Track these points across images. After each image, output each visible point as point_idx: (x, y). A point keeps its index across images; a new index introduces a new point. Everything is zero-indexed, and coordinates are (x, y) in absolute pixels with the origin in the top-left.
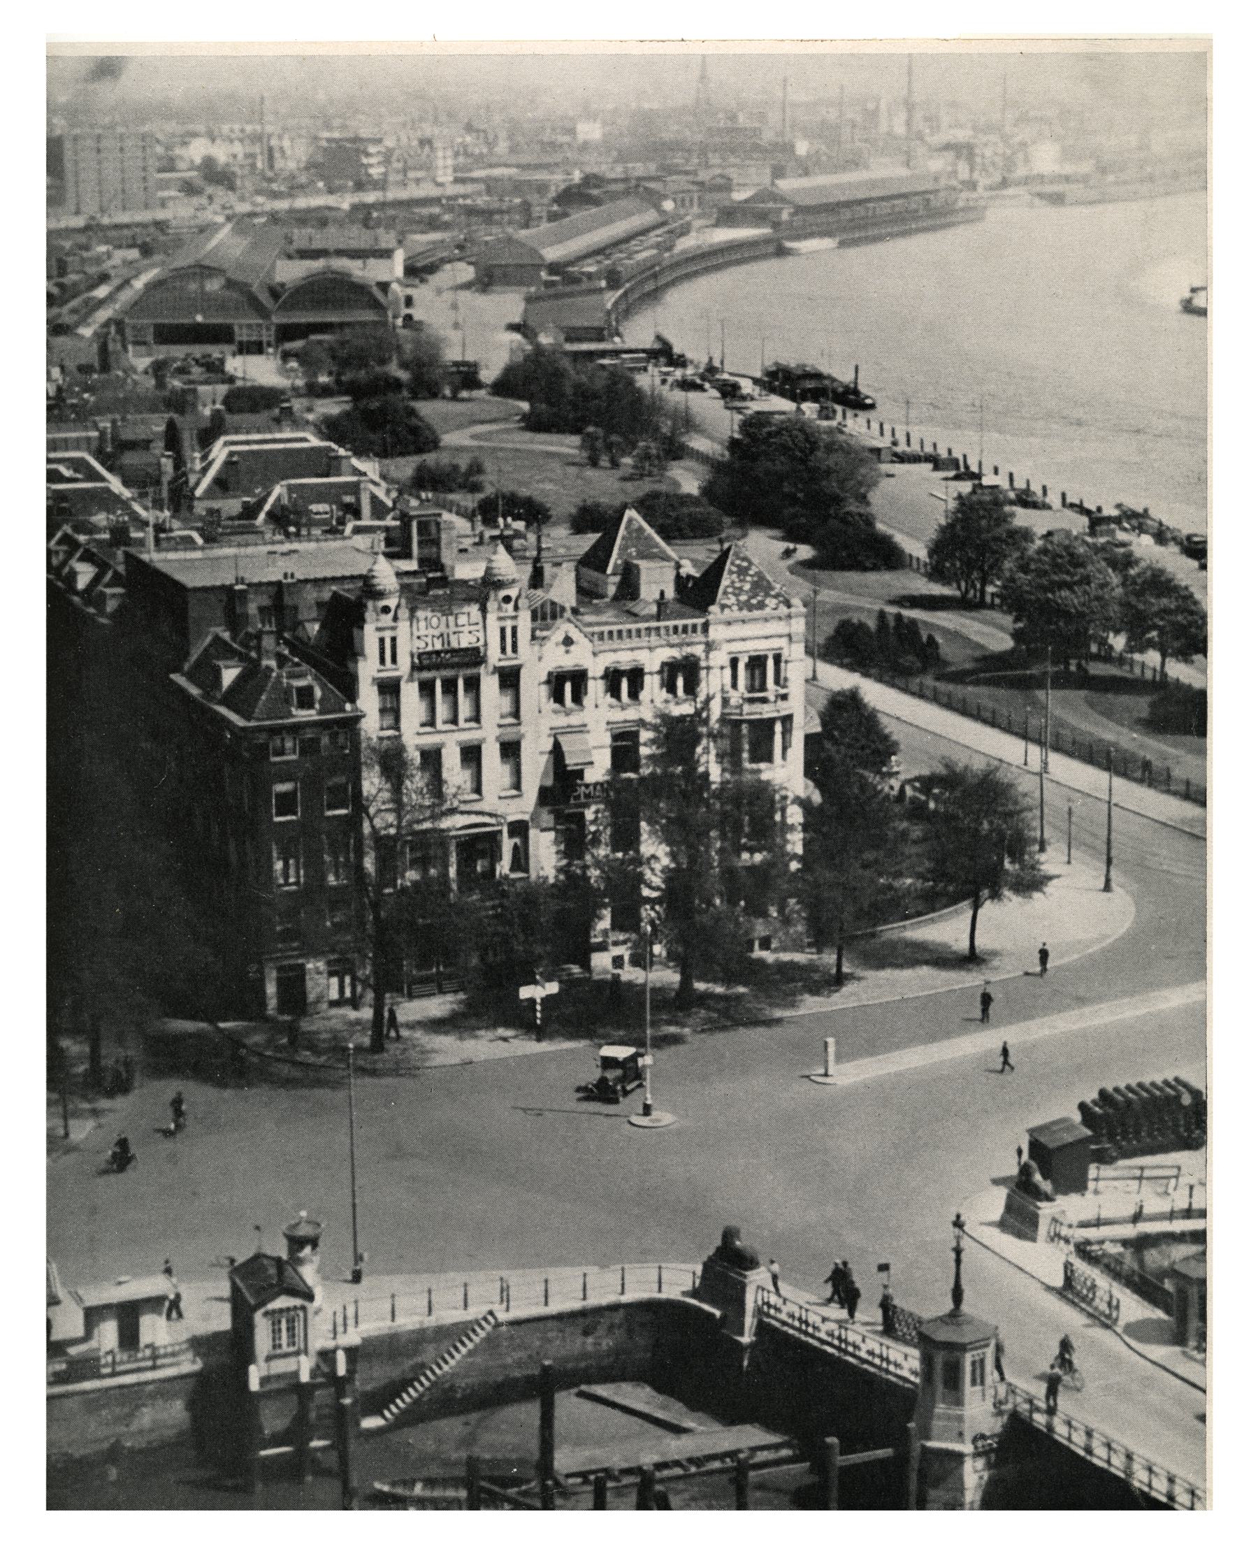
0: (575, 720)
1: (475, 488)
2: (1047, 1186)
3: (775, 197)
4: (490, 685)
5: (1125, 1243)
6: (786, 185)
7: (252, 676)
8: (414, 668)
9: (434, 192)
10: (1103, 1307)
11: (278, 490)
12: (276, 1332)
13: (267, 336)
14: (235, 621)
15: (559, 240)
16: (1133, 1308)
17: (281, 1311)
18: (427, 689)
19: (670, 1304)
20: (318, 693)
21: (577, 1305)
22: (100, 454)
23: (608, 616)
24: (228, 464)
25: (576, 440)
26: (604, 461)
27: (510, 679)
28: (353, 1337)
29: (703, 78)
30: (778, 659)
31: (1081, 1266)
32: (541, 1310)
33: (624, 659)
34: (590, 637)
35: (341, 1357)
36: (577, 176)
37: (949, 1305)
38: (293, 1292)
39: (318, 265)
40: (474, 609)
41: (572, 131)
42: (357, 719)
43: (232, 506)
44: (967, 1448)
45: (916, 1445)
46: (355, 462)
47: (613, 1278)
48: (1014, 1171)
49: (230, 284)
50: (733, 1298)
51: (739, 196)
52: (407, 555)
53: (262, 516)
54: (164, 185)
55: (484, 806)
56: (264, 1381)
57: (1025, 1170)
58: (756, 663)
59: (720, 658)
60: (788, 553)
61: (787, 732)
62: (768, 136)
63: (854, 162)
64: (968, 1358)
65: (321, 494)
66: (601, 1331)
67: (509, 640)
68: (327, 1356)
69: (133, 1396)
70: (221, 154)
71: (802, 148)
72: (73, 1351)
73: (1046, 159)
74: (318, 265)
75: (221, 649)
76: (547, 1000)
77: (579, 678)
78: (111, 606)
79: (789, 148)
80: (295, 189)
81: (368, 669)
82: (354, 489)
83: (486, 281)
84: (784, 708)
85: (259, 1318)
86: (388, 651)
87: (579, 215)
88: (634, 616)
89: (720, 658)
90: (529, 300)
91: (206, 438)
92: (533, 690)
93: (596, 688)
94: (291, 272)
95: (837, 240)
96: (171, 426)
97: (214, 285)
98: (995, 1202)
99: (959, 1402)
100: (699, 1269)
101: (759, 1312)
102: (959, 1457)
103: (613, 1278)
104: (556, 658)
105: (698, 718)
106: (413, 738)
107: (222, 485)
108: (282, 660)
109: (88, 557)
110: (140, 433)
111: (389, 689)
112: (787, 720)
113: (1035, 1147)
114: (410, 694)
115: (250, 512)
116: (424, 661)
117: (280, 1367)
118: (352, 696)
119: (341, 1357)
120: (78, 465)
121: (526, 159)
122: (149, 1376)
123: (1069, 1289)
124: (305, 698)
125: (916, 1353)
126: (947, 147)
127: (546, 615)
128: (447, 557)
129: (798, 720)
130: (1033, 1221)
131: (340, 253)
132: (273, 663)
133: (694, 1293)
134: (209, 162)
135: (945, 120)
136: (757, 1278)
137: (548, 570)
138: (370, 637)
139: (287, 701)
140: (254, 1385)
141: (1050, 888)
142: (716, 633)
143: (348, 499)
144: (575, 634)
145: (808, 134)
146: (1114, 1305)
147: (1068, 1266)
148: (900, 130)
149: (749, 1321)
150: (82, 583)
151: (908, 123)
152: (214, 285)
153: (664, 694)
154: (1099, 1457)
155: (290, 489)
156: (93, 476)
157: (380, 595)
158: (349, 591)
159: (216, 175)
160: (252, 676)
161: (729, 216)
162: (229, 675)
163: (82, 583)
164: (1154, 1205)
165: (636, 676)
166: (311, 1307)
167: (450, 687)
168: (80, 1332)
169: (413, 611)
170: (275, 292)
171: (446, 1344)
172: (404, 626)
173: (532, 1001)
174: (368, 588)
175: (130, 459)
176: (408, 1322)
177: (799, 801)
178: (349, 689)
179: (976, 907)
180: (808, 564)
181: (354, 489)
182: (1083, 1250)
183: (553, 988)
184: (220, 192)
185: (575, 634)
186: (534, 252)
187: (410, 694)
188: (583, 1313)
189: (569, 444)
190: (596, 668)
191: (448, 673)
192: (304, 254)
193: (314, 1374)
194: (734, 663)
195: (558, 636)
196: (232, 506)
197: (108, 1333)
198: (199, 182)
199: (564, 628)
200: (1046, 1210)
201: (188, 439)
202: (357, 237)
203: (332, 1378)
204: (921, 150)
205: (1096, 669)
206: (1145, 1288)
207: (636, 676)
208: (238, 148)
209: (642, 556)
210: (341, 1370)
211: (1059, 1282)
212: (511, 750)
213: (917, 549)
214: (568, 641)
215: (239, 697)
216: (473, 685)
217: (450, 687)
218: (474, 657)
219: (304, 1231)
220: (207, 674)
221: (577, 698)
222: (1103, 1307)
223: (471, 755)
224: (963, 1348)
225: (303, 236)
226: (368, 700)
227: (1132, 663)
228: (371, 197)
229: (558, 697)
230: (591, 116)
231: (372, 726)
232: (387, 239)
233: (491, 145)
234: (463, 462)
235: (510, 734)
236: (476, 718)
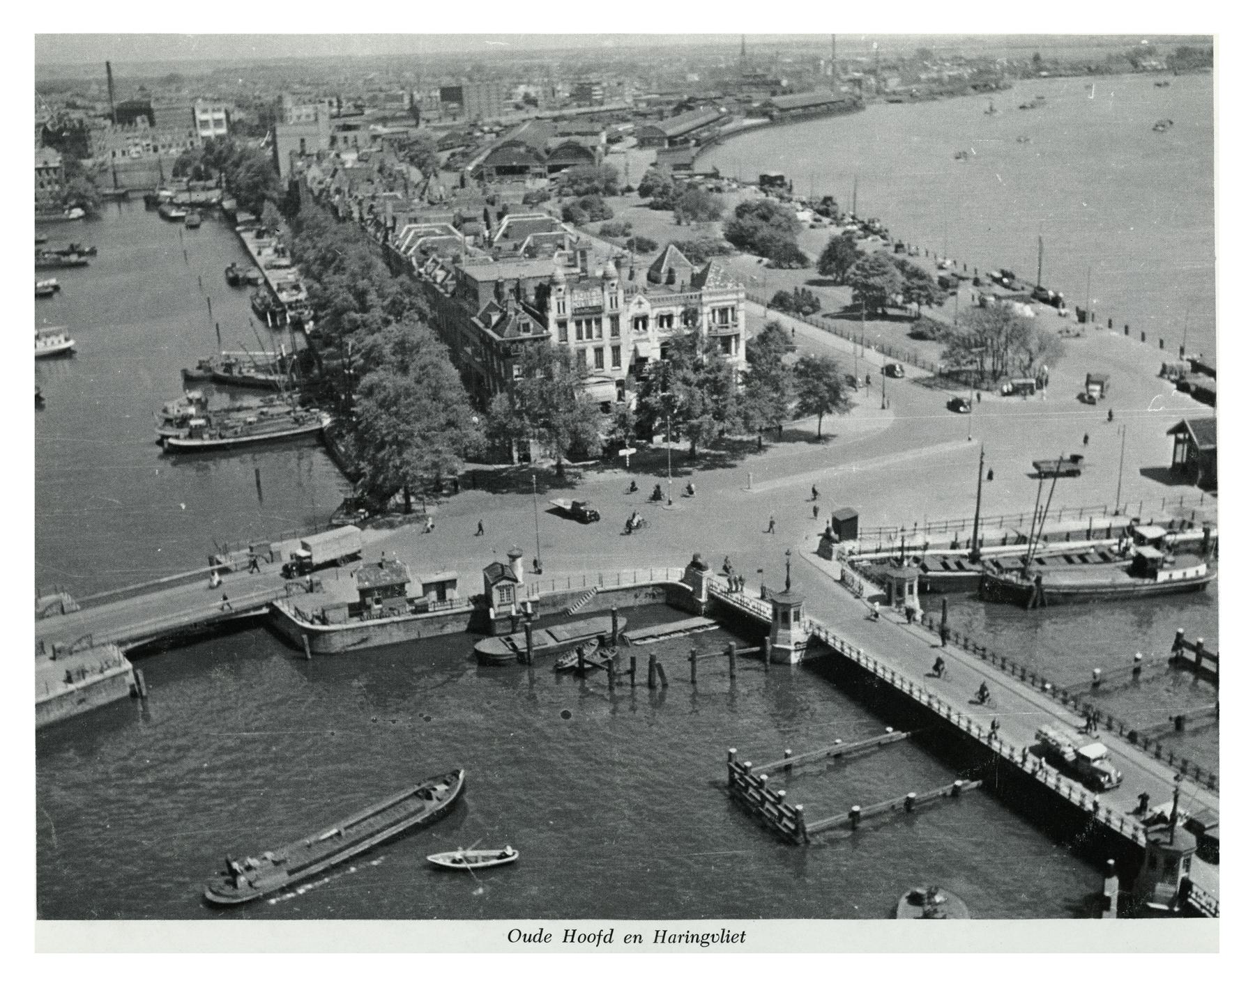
0: (643, 337)
1: (627, 235)
2: (836, 537)
3: (771, 105)
4: (606, 324)
5: (872, 561)
6: (775, 99)
7: (504, 318)
8: (574, 315)
9: (624, 106)
10: (857, 589)
11: (529, 239)
12: (502, 595)
13: (544, 170)
14: (499, 295)
15: (674, 125)
16: (871, 589)
17: (504, 587)
18: (578, 324)
19: (673, 586)
20: (532, 326)
21: (632, 585)
22: (455, 225)
23: (661, 291)
24: (508, 227)
25: (671, 213)
26: (684, 223)
27: (615, 319)
28: (536, 597)
29: (743, 53)
30: (733, 309)
31: (849, 571)
32: (615, 587)
33: (665, 311)
34: (650, 301)
35: (529, 605)
36: (686, 97)
37: (785, 588)
38: (508, 579)
39: (566, 139)
40: (598, 290)
41: (684, 78)
42: (548, 337)
43: (509, 245)
44: (792, 647)
45: (769, 647)
46: (563, 225)
47: (647, 574)
48: (823, 531)
49: (529, 151)
50: (697, 583)
51: (756, 105)
52: (575, 266)
53: (522, 250)
54: (506, 106)
55: (605, 373)
56: (496, 615)
57: (828, 530)
58: (723, 311)
59: (707, 309)
60: (760, 262)
61: (737, 341)
62: (770, 78)
63: (809, 88)
64: (792, 611)
65: (547, 239)
66: (642, 595)
67: (614, 302)
68: (524, 604)
69: (441, 620)
70: (532, 91)
71: (784, 83)
72: (417, 601)
73: (894, 83)
74: (566, 139)
75: (491, 307)
76: (632, 456)
77: (644, 319)
78: (450, 289)
79: (778, 83)
80: (565, 105)
81: (552, 315)
82: (562, 237)
83: (643, 143)
84: (735, 331)
85: (494, 589)
86: (561, 307)
87: (685, 114)
88: (672, 291)
89: (707, 309)
90: (659, 153)
91: (500, 216)
92: (625, 323)
93: (652, 323)
94: (554, 143)
95: (254, 232)
96: (486, 211)
97: (522, 150)
98: (816, 542)
99: (789, 628)
100: (683, 570)
101: (708, 589)
102: (789, 652)
103: (647, 574)
104: (634, 310)
105: (695, 336)
106: (573, 343)
107: (505, 236)
108: (517, 312)
109: (442, 268)
110: (472, 213)
111: (562, 324)
112: (737, 336)
113: (835, 520)
114: (572, 327)
115: (516, 248)
116: (578, 312)
117: (503, 609)
118: (546, 327)
119: (529, 605)
120: (445, 228)
121: (664, 91)
122: (448, 612)
123: (843, 581)
124: (526, 328)
125: (770, 606)
126: (850, 80)
127: (630, 292)
128: (589, 268)
129: (742, 336)
130: (831, 552)
131: (578, 134)
132: (513, 313)
133: (682, 581)
134: (526, 96)
135: (850, 68)
136: (706, 574)
137: (636, 271)
138: (553, 301)
139: (519, 329)
140: (492, 616)
141: (853, 411)
142: (705, 299)
143: (559, 242)
144: (643, 300)
145: (787, 75)
146: (861, 588)
147: (843, 571)
148: (829, 73)
149: (704, 592)
150: (439, 280)
151: (833, 71)
152: (522, 150)
153: (683, 326)
154: (847, 653)
155: (535, 237)
156: (450, 233)
157: (556, 284)
158: (545, 282)
159: (530, 101)
160: (504, 318)
161: (750, 114)
162: (495, 318)
163: (439, 280)
164: (885, 545)
165: (670, 318)
166: (516, 585)
167: (589, 323)
168: (421, 594)
169: (572, 290)
170: (547, 152)
171: (576, 600)
172: (568, 297)
173: (624, 457)
174: (553, 282)
175: (467, 225)
176: (560, 589)
177: (742, 372)
178: (544, 322)
179: (821, 416)
180: (768, 266)
181: (562, 237)
182: (852, 563)
183: (633, 451)
184: (532, 108)
185: (643, 300)
186: (662, 132)
187: (572, 327)
188: (634, 588)
189: (668, 215)
190: (653, 314)
191: (588, 317)
192: (563, 134)
193: (518, 612)
194: (713, 311)
195: (636, 301)
196: (509, 245)
197: (433, 595)
198: (522, 104)
199: (638, 297)
200: (836, 547)
201: (493, 217)
202: (586, 127)
203: (526, 615)
204: (838, 83)
205: (890, 311)
206: (880, 581)
207: (670, 318)
208: (539, 88)
209: (677, 265)
210: (530, 611)
211: (839, 578)
212: (616, 349)
213: (814, 257)
214: (640, 303)
215: (498, 328)
216: (599, 321)
217: (589, 323)
218: (598, 310)
219: (515, 553)
220: (486, 319)
221: (645, 327)
222: (857, 589)
223: (599, 351)
224: (789, 606)
225: (563, 126)
226: (553, 328)
227: (906, 309)
228: (596, 109)
229: (636, 327)
230: (692, 70)
231: (555, 339)
232: (598, 127)
233: (649, 84)
234: (622, 223)
235: (615, 343)
236: (600, 336)
